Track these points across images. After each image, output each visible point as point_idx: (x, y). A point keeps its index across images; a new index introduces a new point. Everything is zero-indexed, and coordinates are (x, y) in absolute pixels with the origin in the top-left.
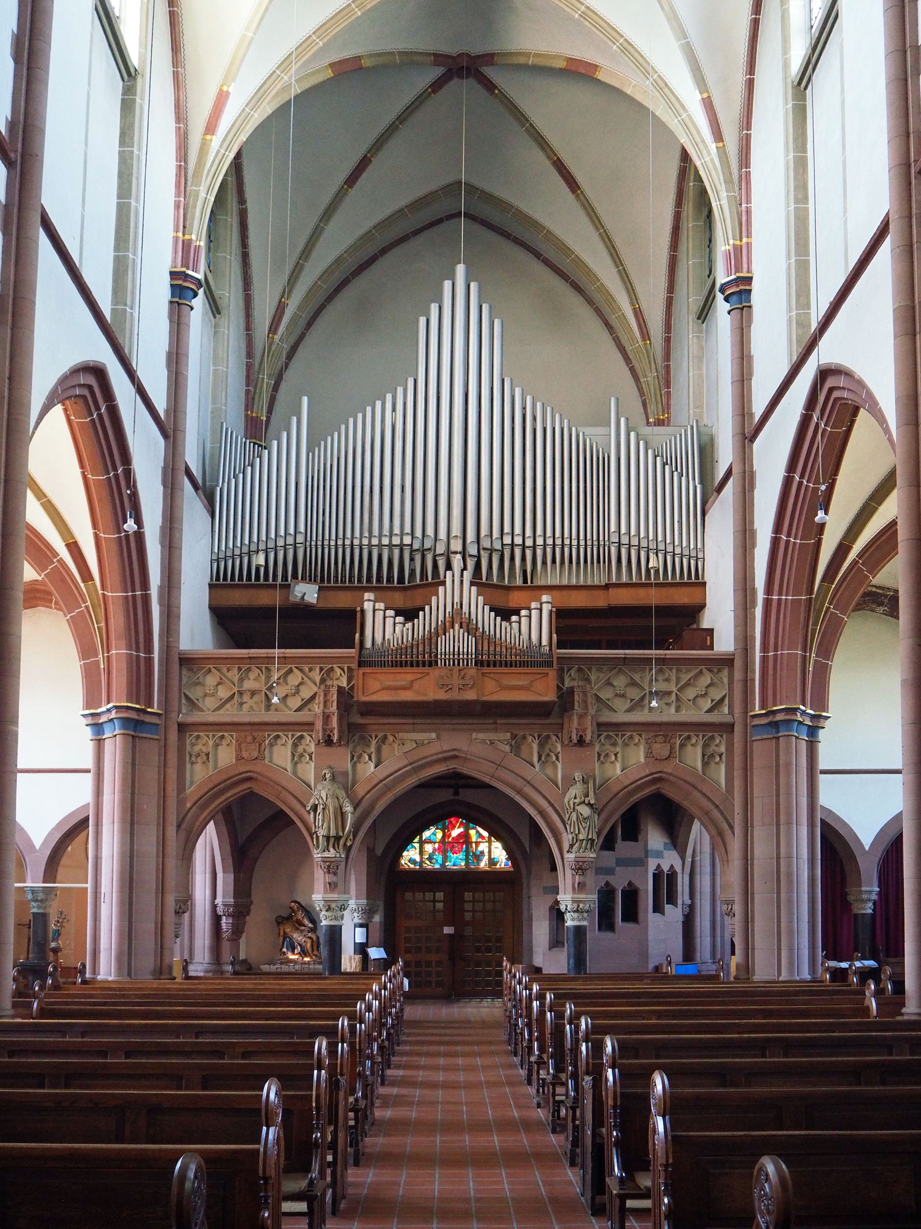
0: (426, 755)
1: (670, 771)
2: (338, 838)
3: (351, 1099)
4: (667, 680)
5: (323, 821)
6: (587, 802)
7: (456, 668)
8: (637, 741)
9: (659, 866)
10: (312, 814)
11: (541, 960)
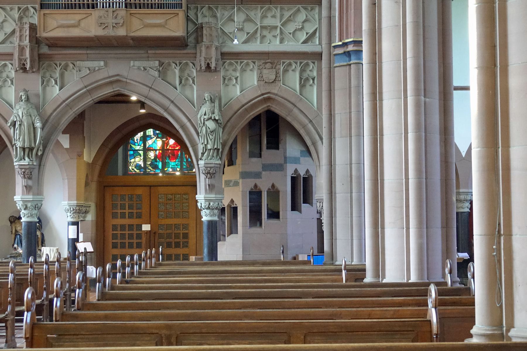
1: (276, 92)
2: (31, 149)
4: (274, 17)
5: (20, 135)
7: (111, 9)
8: (252, 67)
9: (296, 171)
10: (12, 129)
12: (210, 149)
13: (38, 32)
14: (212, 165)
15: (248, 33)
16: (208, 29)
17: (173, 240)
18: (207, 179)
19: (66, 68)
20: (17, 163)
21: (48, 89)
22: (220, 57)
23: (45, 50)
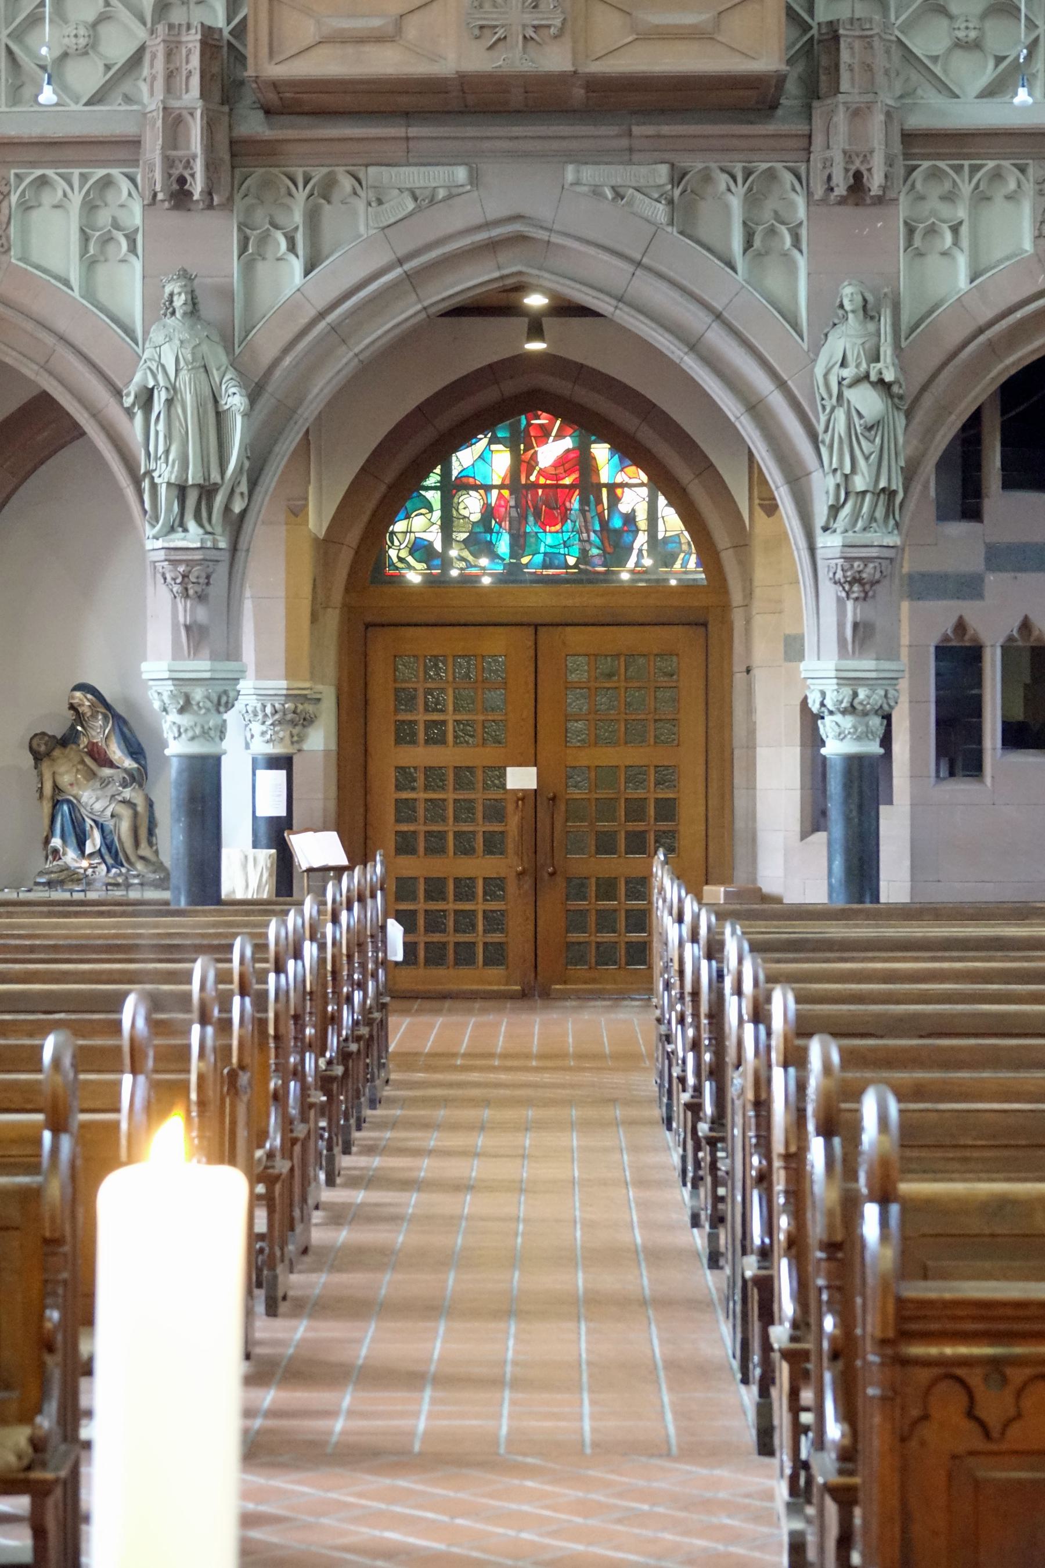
0: (440, 234)
2: (207, 492)
3: (259, 1153)
5: (169, 437)
6: (873, 377)
8: (1012, 185)
11: (780, 872)
12: (864, 493)
13: (250, 61)
14: (873, 552)
15: (999, 60)
16: (857, 44)
17: (621, 827)
18: (850, 605)
19: (327, 190)
20: (159, 544)
21: (261, 267)
22: (897, 148)
23: (253, 125)
